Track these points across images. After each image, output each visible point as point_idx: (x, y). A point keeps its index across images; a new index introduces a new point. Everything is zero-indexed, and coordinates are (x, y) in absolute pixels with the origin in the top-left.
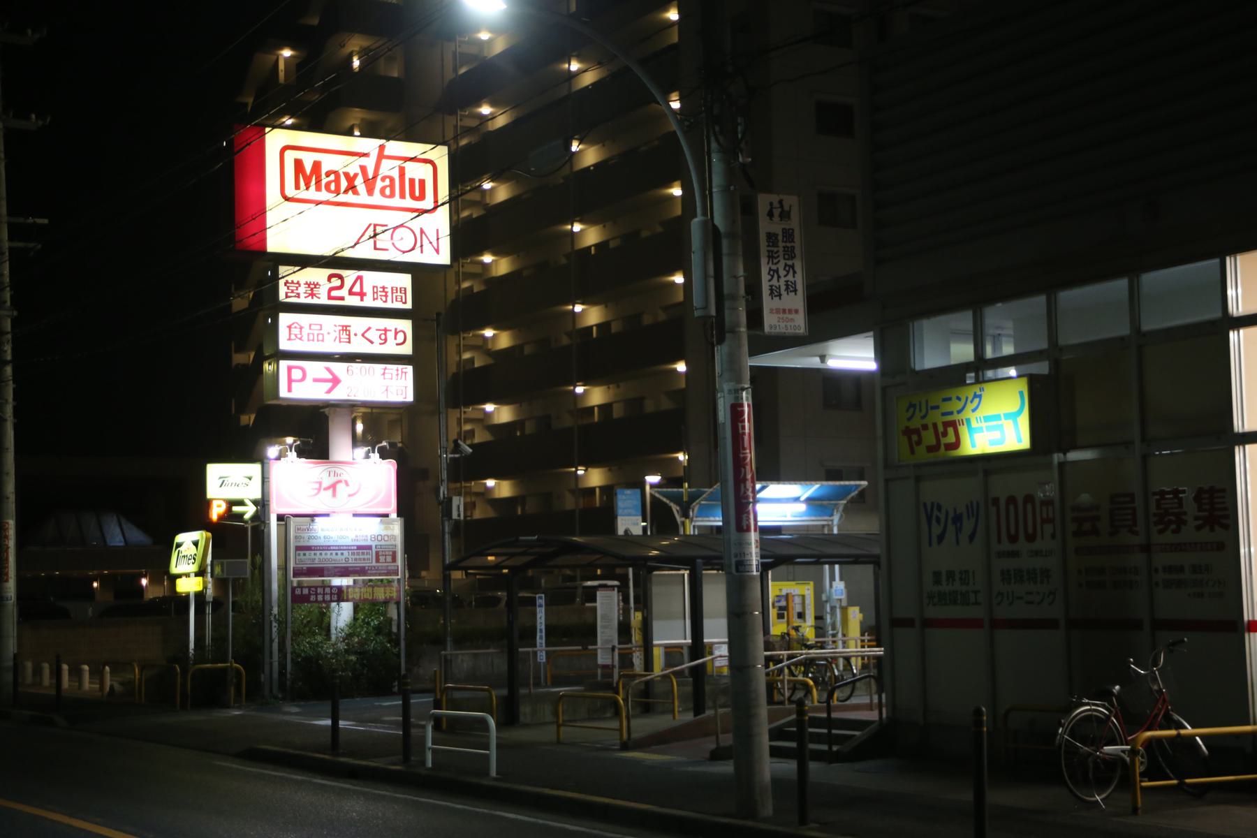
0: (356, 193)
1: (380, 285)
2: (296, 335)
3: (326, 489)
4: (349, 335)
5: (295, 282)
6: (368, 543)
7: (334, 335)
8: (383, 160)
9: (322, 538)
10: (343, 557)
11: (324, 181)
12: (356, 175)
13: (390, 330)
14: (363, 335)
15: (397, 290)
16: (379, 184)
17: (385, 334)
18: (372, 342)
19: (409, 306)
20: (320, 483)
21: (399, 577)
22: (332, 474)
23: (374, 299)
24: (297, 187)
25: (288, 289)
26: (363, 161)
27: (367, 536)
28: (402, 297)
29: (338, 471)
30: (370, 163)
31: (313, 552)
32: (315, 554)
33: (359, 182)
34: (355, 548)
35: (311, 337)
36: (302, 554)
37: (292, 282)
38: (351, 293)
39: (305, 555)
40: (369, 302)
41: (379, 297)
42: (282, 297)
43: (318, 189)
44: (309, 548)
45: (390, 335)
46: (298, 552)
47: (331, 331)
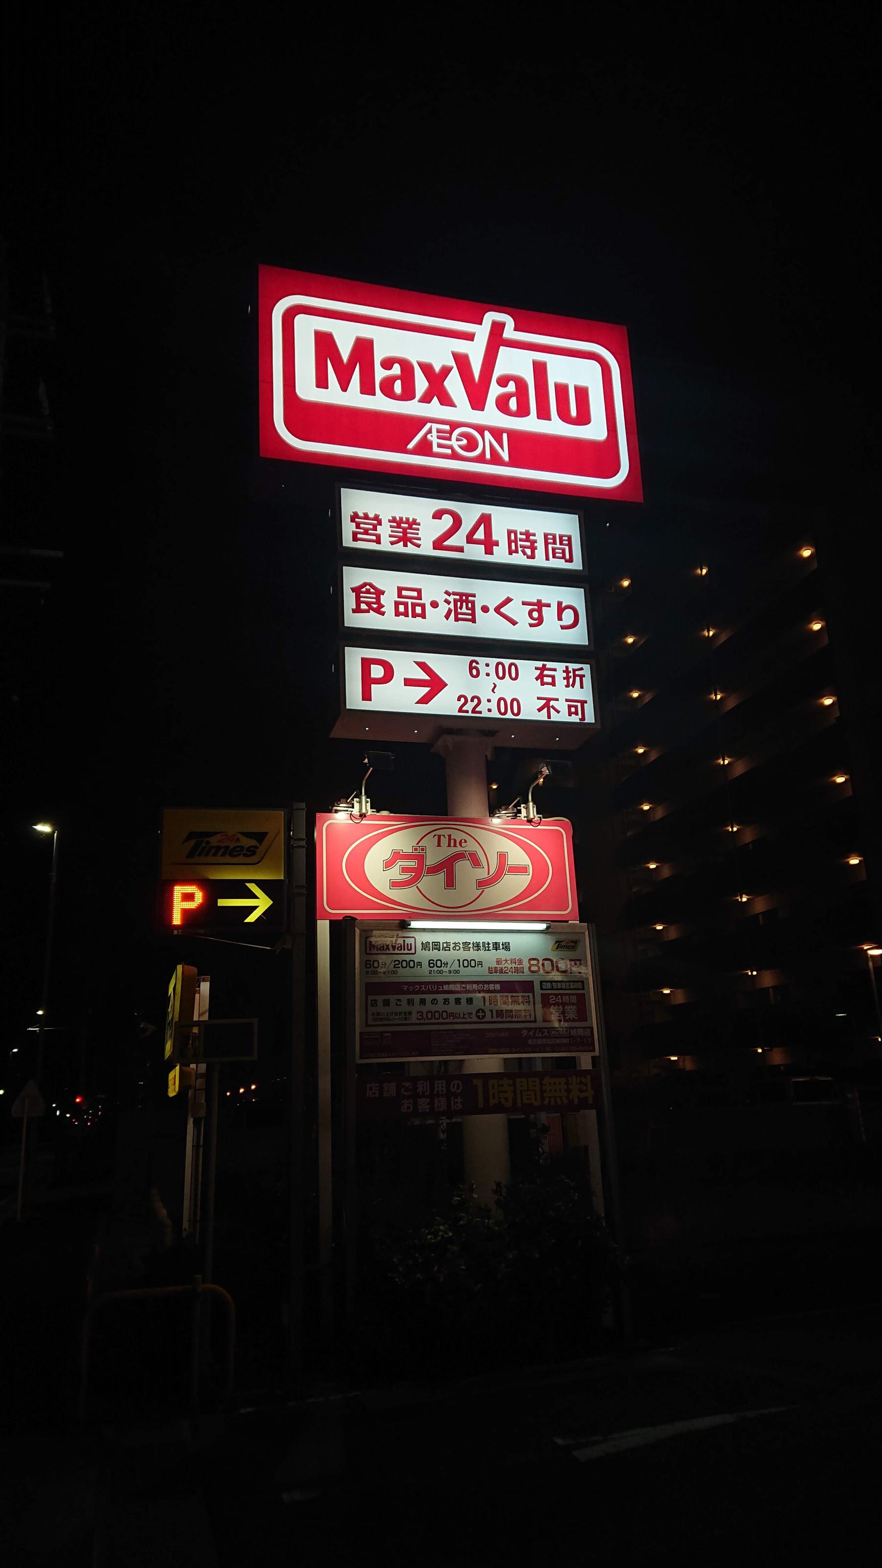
0: (446, 401)
1: (520, 529)
2: (368, 604)
3: (433, 870)
4: (473, 609)
5: (371, 515)
6: (525, 977)
7: (443, 608)
8: (502, 348)
9: (425, 964)
10: (472, 1009)
11: (380, 374)
12: (446, 371)
13: (548, 605)
14: (497, 610)
15: (554, 538)
16: (495, 391)
17: (540, 611)
18: (514, 623)
19: (577, 564)
20: (421, 858)
21: (597, 1053)
22: (444, 841)
23: (511, 553)
24: (322, 382)
25: (358, 526)
26: (461, 346)
27: (520, 961)
28: (564, 551)
29: (458, 836)
30: (476, 350)
31: (404, 998)
32: (410, 1002)
33: (454, 384)
34: (498, 987)
35: (402, 608)
36: (380, 1004)
37: (366, 516)
38: (470, 539)
39: (387, 1003)
40: (501, 555)
41: (520, 549)
42: (348, 541)
43: (367, 388)
44: (398, 988)
45: (550, 614)
46: (370, 998)
47: (440, 599)
